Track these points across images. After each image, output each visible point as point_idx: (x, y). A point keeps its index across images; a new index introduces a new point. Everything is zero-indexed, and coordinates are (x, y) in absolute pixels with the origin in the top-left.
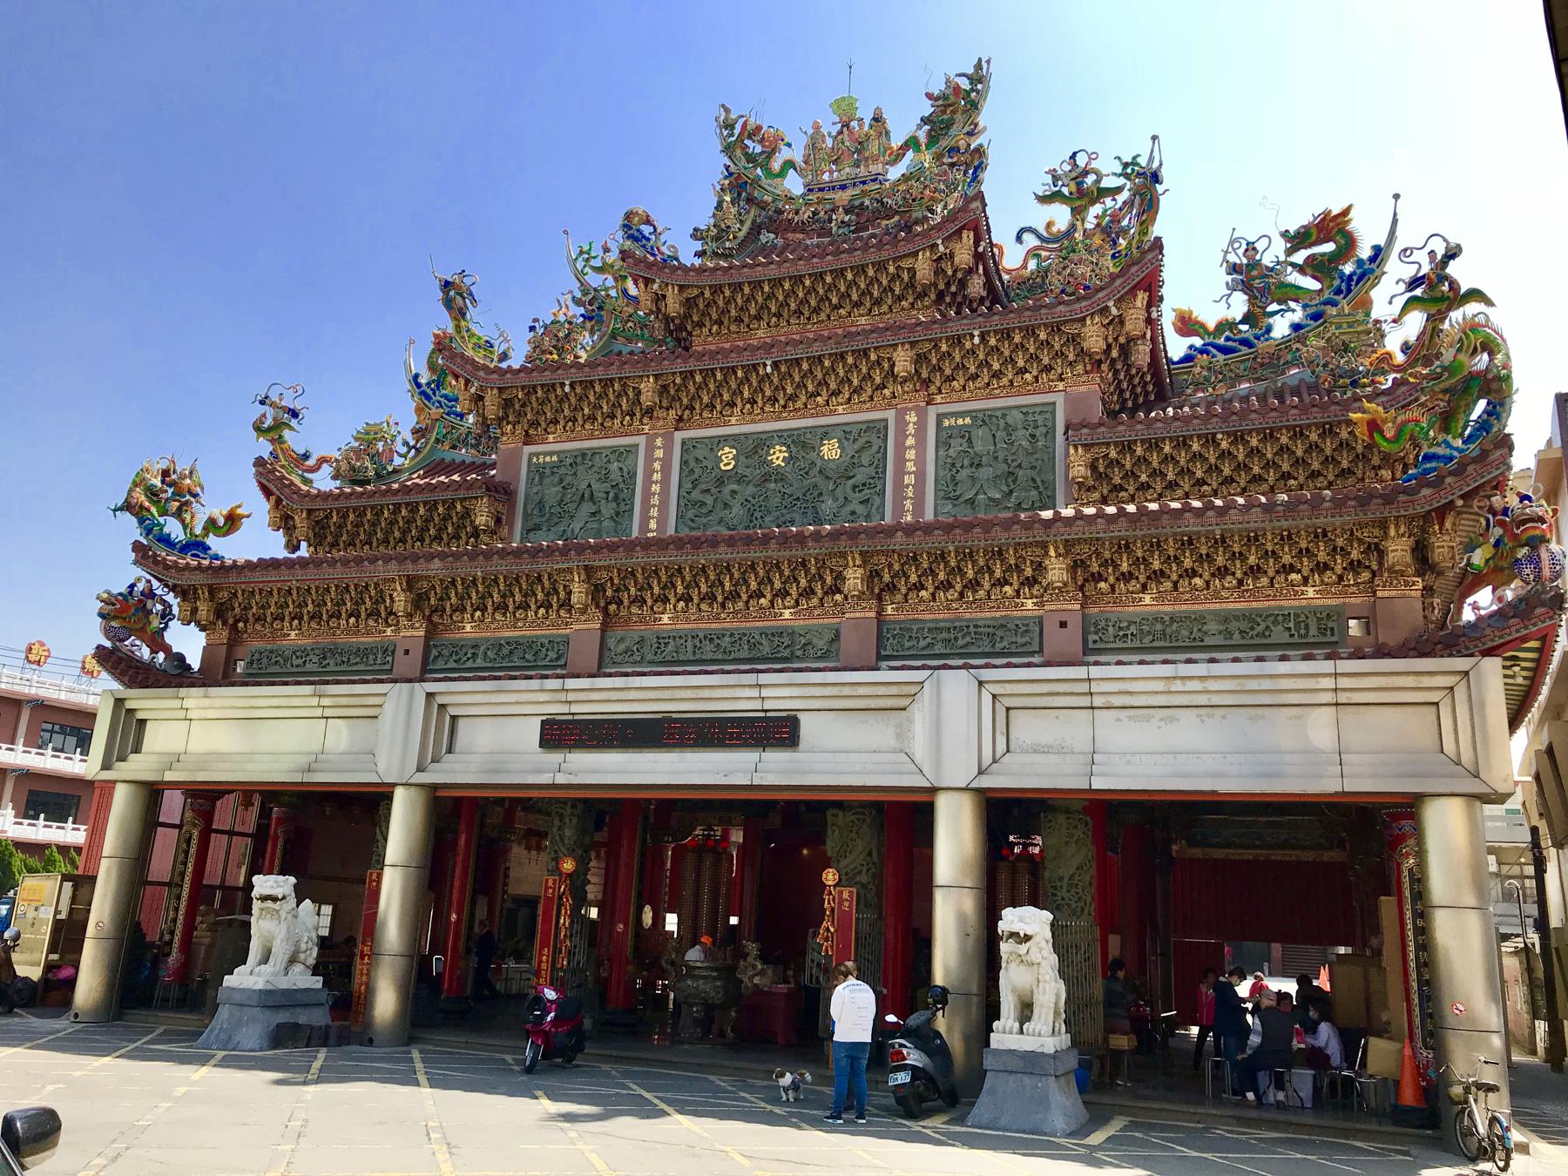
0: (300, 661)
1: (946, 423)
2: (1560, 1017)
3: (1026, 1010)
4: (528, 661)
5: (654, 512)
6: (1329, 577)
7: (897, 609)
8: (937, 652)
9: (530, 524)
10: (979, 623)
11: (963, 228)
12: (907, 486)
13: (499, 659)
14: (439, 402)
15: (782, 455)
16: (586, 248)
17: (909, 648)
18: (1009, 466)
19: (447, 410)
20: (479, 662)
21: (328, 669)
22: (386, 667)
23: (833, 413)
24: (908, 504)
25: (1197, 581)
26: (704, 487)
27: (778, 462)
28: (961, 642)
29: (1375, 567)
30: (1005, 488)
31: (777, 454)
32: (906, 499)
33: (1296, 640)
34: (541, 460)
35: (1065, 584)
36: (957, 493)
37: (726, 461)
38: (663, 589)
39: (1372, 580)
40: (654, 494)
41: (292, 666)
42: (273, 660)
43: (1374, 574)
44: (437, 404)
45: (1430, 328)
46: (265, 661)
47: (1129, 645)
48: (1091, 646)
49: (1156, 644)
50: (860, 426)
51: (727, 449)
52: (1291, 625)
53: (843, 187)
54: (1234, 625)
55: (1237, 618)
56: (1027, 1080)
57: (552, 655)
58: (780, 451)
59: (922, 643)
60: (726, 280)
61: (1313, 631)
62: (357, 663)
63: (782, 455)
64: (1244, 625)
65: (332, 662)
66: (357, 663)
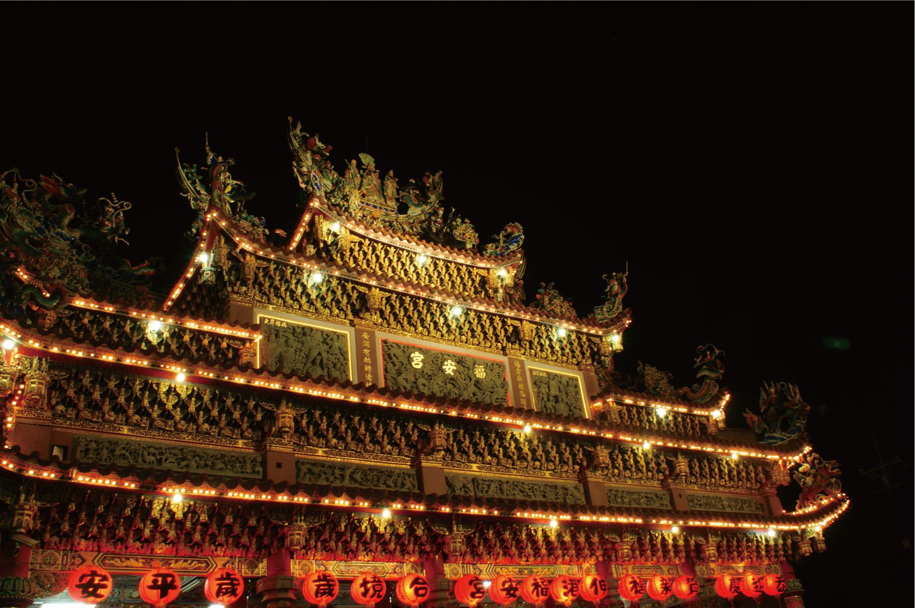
0: (152, 458)
4: (356, 481)
37: (416, 362)
40: (367, 372)
41: (144, 461)
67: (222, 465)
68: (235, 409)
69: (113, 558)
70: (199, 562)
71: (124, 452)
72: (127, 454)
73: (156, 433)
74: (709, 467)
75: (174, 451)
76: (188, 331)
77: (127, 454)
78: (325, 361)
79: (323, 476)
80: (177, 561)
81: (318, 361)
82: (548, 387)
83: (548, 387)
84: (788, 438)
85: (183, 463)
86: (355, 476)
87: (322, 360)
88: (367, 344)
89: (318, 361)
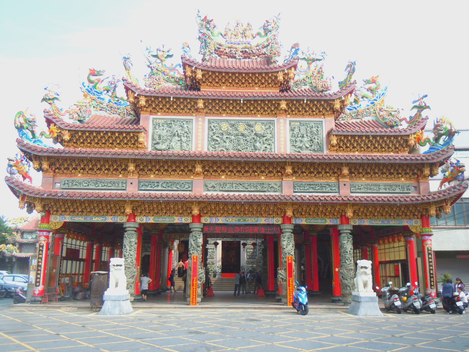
0: (86, 185)
1: (292, 124)
2: (450, 296)
3: (365, 285)
4: (164, 187)
5: (200, 142)
6: (408, 176)
7: (296, 178)
8: (310, 191)
9: (155, 142)
10: (322, 183)
11: (292, 66)
12: (282, 141)
13: (167, 187)
14: (94, 93)
15: (242, 128)
16: (149, 48)
17: (318, 190)
18: (311, 138)
19: (98, 96)
20: (160, 188)
21: (98, 188)
22: (123, 188)
23: (256, 116)
24: (282, 146)
25: (256, 174)
26: (217, 135)
27: (241, 130)
28: (317, 188)
29: (339, 173)
30: (310, 144)
31: (241, 128)
32: (281, 145)
33: (401, 191)
34: (158, 121)
35: (134, 171)
36: (296, 144)
37: (224, 128)
38: (68, 165)
39: (338, 177)
40: (199, 136)
41: (83, 186)
42: (74, 184)
43: (339, 175)
44: (93, 94)
45: (419, 113)
46: (70, 184)
47: (362, 191)
48: (352, 191)
49: (368, 191)
50: (267, 122)
51: (224, 124)
52: (400, 188)
53: (239, 44)
54: (387, 187)
55: (388, 185)
56: (372, 303)
57: (187, 186)
58: (242, 127)
59: (306, 188)
60: (217, 70)
61: (405, 189)
62: (110, 186)
63: (243, 128)
64: (389, 187)
65: (100, 185)
66: (110, 186)
67: (111, 185)
68: (384, 169)
69: (74, 217)
70: (103, 218)
71: (76, 183)
72: (78, 184)
73: (90, 175)
74: (262, 55)
75: (93, 181)
76: (344, 164)
77: (78, 184)
78: (179, 134)
79: (150, 186)
80: (95, 218)
81: (176, 135)
82: (299, 130)
83: (299, 130)
84: (442, 148)
85: (97, 185)
86: (163, 185)
87: (178, 134)
88: (282, 143)
89: (176, 135)
